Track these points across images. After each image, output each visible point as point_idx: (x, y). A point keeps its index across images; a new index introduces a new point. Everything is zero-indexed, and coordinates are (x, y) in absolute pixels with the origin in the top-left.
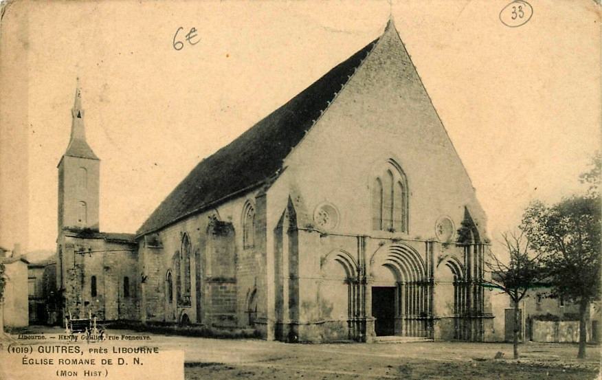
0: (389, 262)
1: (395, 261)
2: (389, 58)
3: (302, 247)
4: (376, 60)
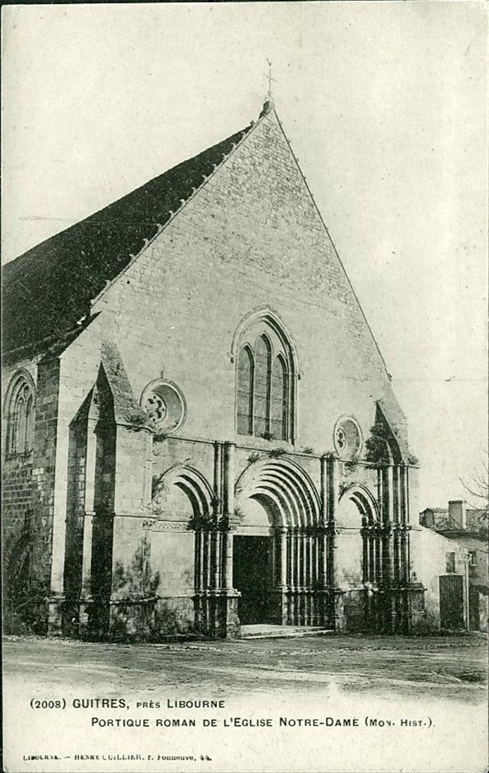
0: (260, 491)
1: (272, 490)
2: (267, 157)
3: (121, 457)
4: (248, 158)
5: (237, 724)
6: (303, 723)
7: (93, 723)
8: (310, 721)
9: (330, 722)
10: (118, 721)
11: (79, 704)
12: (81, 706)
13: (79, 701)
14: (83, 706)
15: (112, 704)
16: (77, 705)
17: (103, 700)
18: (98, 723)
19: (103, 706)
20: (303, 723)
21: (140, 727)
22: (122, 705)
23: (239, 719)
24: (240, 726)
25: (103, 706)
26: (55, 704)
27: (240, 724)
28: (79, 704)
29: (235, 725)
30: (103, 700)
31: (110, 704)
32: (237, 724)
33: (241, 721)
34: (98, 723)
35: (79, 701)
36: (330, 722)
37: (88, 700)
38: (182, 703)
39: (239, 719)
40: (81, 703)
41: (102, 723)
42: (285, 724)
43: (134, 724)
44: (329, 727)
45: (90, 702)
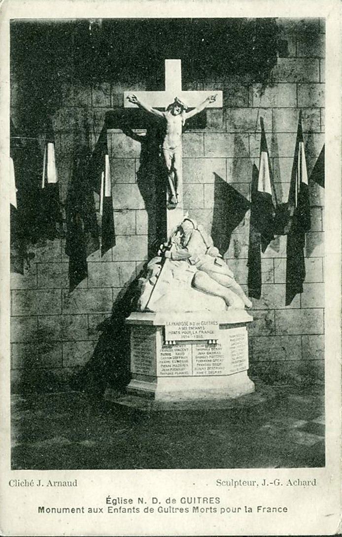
6: (201, 500)
8: (207, 499)
10: (199, 498)
11: (162, 510)
12: (164, 512)
13: (184, 498)
14: (55, 509)
15: (210, 501)
16: (183, 502)
19: (204, 503)
20: (201, 500)
21: (173, 498)
22: (218, 502)
23: (261, 507)
24: (112, 512)
25: (204, 503)
27: (111, 502)
28: (162, 510)
29: (107, 503)
32: (110, 511)
33: (111, 500)
34: (225, 509)
38: (205, 499)
39: (261, 507)
40: (186, 500)
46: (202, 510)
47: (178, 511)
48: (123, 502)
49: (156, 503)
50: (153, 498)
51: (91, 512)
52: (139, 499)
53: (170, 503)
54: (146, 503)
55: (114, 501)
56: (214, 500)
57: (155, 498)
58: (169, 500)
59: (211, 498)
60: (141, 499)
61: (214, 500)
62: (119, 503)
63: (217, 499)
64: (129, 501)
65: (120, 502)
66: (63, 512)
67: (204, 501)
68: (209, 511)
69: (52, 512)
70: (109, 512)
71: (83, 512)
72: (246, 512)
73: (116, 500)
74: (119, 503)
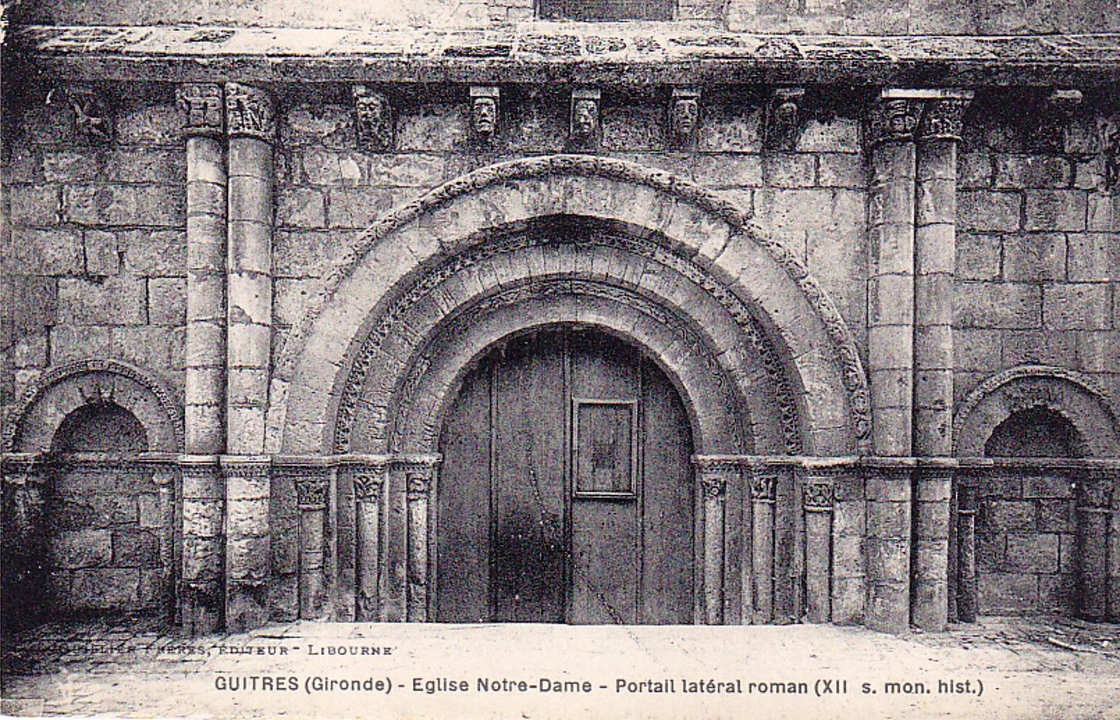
5: (417, 687)
7: (618, 686)
8: (271, 681)
9: (545, 685)
10: (254, 678)
13: (321, 680)
15: (278, 684)
16: (221, 686)
17: (264, 678)
18: (626, 687)
19: (264, 688)
20: (259, 683)
22: (293, 686)
25: (264, 688)
26: (553, 686)
30: (264, 678)
31: (274, 684)
34: (626, 687)
35: (321, 680)
36: (545, 685)
37: (800, 692)
40: (227, 682)
41: (632, 687)
42: (486, 689)
43: (228, 686)
44: (544, 693)
45: (669, 683)
46: (496, 686)
47: (515, 688)
48: (448, 687)
49: (548, 690)
50: (751, 685)
51: (733, 691)
52: (480, 680)
53: (371, 689)
54: (874, 692)
55: (430, 686)
56: (286, 682)
57: (547, 680)
58: (371, 682)
59: (278, 679)
60: (481, 687)
61: (287, 684)
62: (440, 690)
63: (293, 681)
64: (461, 686)
65: (442, 686)
66: (566, 690)
67: (264, 684)
68: (645, 689)
69: (771, 691)
70: (415, 690)
71: (740, 691)
72: (685, 691)
73: (433, 683)
74: (440, 690)
